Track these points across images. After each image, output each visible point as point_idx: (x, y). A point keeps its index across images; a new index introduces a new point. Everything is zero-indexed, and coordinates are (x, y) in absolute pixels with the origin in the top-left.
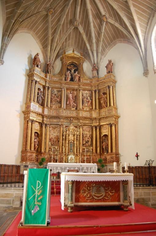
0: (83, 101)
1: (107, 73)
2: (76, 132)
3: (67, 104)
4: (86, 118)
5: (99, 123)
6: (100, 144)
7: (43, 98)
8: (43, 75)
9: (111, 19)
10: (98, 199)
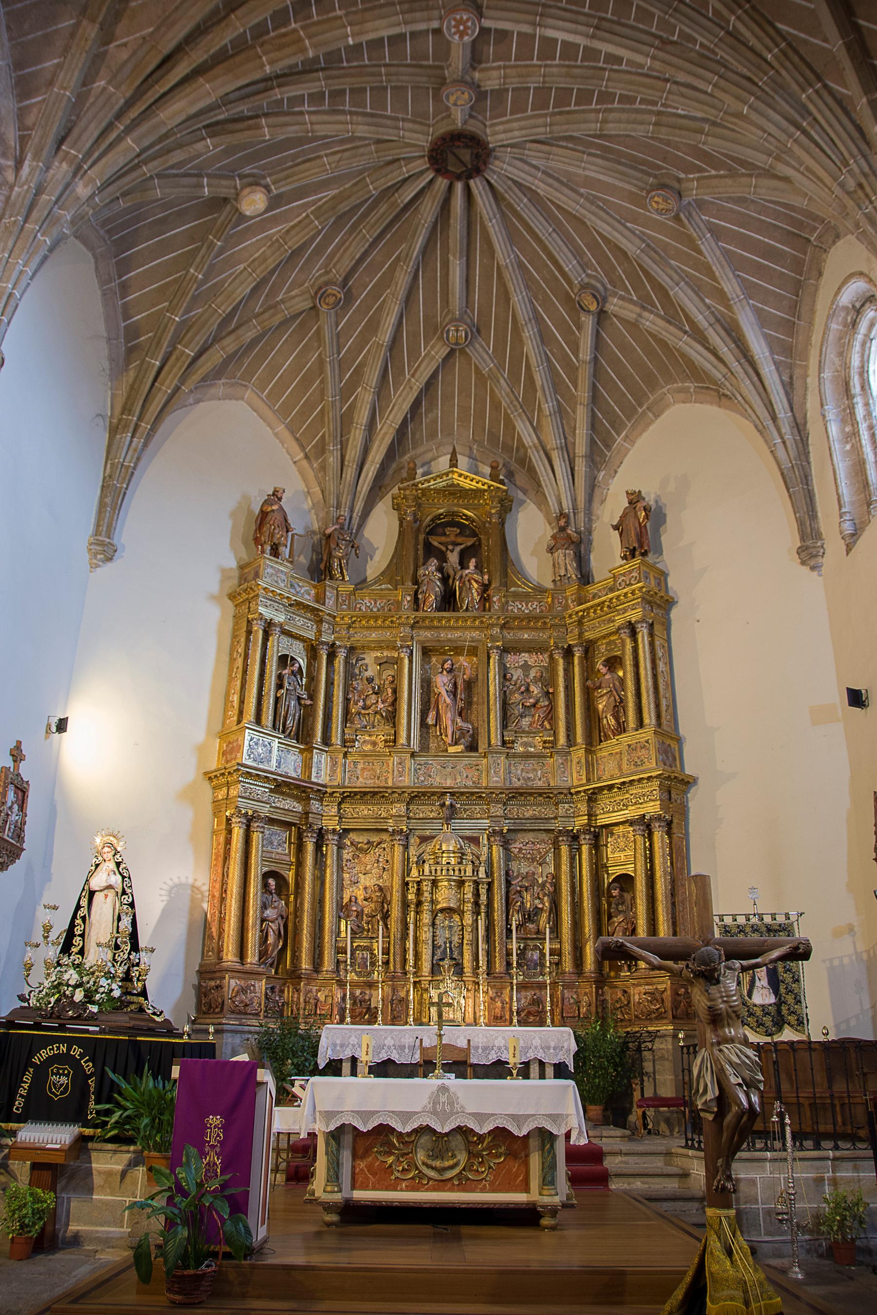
0: (505, 705)
1: (625, 558)
2: (469, 869)
3: (423, 724)
4: (521, 794)
5: (591, 815)
6: (648, 909)
7: (309, 702)
8: (306, 593)
9: (622, 298)
10: (440, 1178)
